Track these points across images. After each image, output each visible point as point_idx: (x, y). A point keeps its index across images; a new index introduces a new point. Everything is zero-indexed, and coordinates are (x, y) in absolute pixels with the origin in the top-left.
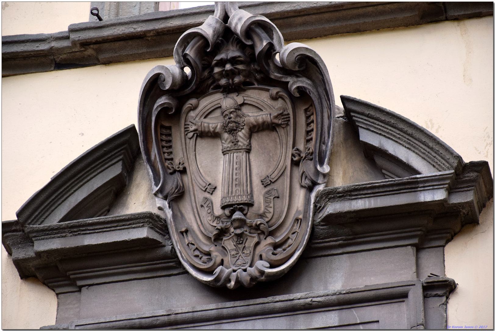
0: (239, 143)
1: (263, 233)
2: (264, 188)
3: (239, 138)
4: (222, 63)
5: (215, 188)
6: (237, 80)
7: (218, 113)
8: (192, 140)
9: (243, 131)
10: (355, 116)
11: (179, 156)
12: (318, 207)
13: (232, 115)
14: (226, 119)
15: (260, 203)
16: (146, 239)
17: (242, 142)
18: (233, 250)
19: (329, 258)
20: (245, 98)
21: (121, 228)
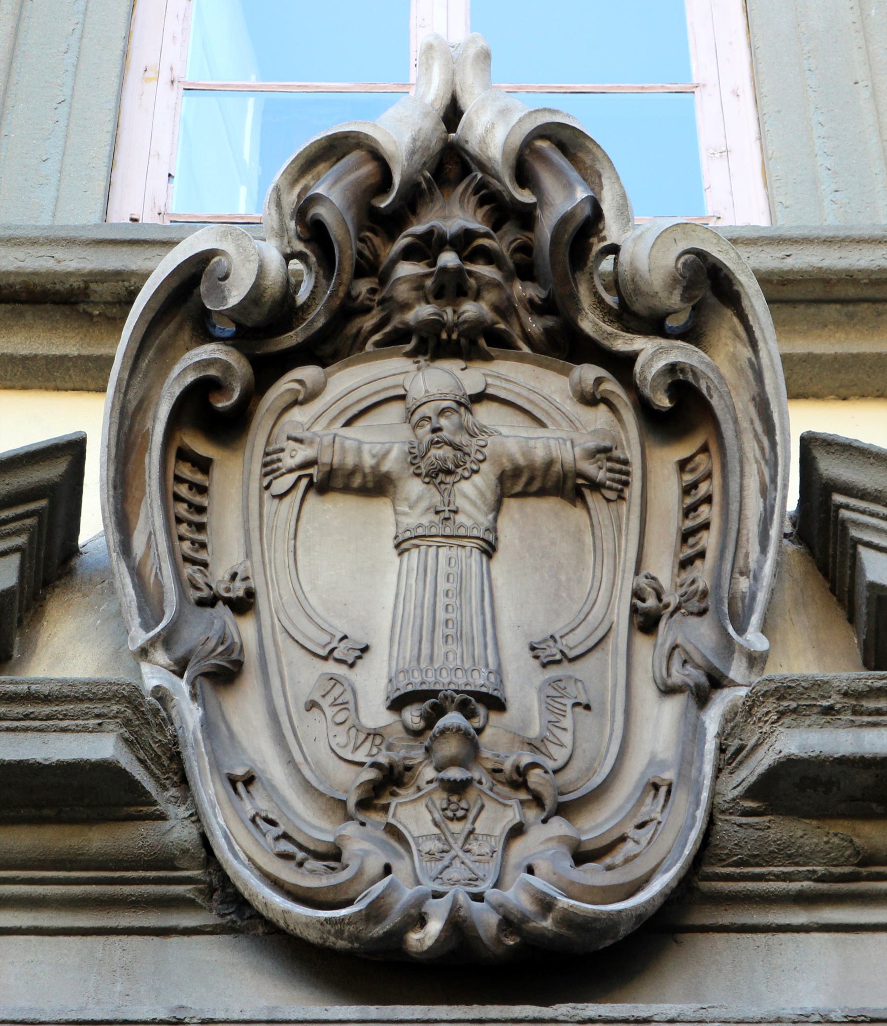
0: (460, 518)
1: (538, 800)
2: (539, 669)
3: (460, 502)
4: (425, 248)
5: (365, 649)
6: (470, 309)
7: (395, 411)
8: (287, 500)
9: (476, 478)
10: (847, 507)
11: (228, 557)
12: (731, 750)
13: (443, 422)
14: (420, 432)
15: (529, 710)
16: (106, 770)
17: (469, 516)
18: (428, 837)
19: (760, 938)
20: (490, 381)
21: (16, 724)
